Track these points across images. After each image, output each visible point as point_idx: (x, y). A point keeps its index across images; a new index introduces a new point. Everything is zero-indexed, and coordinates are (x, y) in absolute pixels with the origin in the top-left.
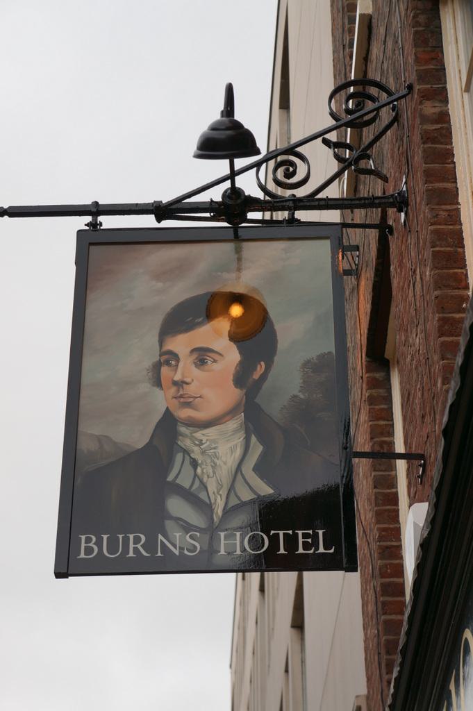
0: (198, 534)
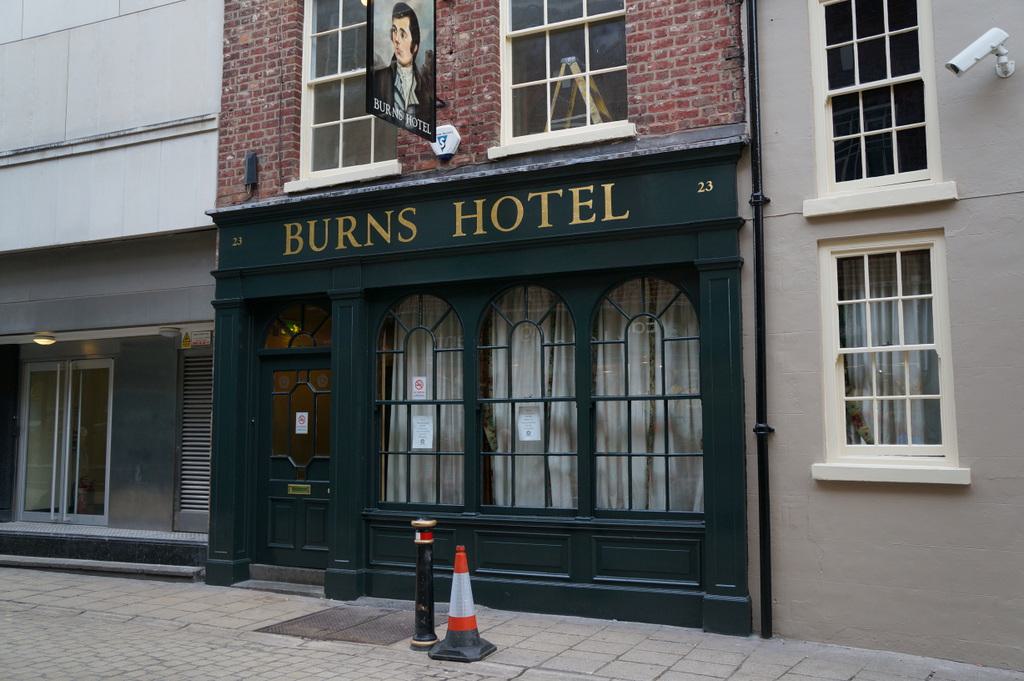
0: (414, 210)
